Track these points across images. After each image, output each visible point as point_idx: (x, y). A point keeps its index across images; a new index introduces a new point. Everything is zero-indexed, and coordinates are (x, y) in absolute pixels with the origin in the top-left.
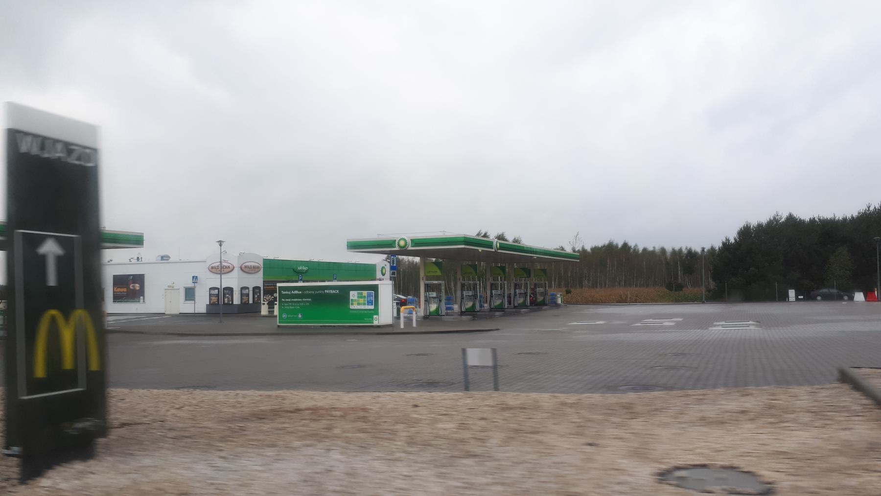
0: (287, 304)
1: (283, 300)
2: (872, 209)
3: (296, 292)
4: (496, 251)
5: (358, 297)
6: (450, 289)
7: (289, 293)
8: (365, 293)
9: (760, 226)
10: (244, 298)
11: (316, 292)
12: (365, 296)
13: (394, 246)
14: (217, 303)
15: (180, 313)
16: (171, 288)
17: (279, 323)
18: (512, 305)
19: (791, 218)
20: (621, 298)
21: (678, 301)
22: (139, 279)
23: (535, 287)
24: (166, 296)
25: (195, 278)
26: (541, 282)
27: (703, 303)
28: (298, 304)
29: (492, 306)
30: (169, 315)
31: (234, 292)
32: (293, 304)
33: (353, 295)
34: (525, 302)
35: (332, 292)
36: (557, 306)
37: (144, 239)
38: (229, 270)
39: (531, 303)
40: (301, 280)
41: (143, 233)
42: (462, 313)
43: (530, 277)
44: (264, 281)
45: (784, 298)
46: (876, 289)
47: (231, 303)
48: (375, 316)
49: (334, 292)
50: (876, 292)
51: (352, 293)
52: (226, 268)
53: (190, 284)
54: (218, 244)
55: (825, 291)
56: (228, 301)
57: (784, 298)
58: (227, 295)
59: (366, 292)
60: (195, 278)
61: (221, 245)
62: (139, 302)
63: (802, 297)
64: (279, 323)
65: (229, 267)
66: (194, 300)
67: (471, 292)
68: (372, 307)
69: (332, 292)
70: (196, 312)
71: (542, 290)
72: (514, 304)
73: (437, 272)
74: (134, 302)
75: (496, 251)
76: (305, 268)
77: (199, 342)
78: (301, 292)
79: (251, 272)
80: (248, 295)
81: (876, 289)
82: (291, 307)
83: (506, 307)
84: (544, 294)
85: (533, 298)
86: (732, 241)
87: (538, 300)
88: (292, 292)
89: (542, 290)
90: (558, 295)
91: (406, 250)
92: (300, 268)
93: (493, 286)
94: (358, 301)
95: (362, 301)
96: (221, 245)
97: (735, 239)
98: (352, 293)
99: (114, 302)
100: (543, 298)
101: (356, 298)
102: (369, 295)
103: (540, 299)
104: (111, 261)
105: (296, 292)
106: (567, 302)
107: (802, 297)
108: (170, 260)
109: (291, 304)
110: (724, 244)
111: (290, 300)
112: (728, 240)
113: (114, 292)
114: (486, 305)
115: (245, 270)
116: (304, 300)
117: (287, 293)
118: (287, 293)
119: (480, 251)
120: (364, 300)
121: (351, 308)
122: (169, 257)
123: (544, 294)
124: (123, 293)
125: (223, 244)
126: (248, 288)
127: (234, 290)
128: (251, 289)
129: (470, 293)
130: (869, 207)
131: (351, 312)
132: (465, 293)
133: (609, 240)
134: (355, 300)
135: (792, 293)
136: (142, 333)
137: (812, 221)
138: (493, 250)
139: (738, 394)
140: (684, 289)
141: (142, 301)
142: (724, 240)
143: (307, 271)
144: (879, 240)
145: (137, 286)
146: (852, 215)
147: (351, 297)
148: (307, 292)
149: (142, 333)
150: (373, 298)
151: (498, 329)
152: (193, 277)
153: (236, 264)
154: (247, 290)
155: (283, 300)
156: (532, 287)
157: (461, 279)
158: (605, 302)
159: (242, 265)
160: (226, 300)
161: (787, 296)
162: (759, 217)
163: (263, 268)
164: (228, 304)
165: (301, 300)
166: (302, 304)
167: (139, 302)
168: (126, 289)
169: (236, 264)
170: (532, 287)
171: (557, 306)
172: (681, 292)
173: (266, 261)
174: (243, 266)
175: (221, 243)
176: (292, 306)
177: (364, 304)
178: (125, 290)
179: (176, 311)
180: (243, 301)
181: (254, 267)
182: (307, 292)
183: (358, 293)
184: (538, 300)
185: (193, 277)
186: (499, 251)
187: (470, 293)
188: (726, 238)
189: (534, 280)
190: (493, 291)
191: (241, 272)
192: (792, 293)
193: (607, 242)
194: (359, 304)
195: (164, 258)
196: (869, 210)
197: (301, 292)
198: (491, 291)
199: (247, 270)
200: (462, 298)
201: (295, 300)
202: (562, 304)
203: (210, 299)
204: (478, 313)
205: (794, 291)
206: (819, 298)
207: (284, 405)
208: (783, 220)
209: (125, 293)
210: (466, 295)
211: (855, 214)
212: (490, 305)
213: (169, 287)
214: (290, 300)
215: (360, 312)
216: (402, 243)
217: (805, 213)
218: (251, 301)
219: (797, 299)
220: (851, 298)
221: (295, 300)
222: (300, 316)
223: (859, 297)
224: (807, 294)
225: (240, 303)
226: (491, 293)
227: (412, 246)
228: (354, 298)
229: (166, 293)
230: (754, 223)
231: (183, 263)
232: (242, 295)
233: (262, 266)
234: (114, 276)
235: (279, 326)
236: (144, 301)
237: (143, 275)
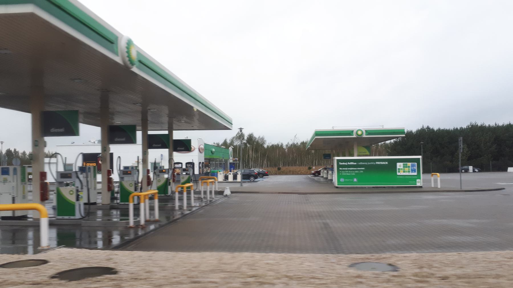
3: (352, 163)
5: (404, 167)
8: (409, 164)
11: (369, 163)
12: (409, 166)
13: (352, 134)
19: (428, 128)
28: (354, 172)
32: (350, 172)
33: (399, 165)
35: (382, 163)
44: (205, 159)
48: (418, 180)
61: (2, 144)
68: (416, 174)
69: (382, 163)
73: (366, 152)
78: (355, 164)
82: (348, 174)
91: (362, 137)
94: (404, 169)
95: (407, 169)
96: (2, 144)
101: (402, 167)
102: (412, 166)
105: (352, 163)
116: (343, 169)
120: (409, 169)
125: (4, 143)
126: (181, 163)
127: (195, 164)
131: (398, 177)
134: (401, 169)
135: (471, 168)
147: (398, 167)
148: (361, 163)
150: (416, 168)
154: (181, 165)
155: (340, 169)
168: (95, 164)
177: (409, 172)
182: (361, 163)
183: (404, 164)
194: (404, 172)
197: (355, 164)
205: (472, 167)
211: (436, 129)
214: (346, 169)
215: (406, 177)
216: (360, 133)
217: (435, 127)
219: (474, 171)
222: (355, 180)
227: (366, 135)
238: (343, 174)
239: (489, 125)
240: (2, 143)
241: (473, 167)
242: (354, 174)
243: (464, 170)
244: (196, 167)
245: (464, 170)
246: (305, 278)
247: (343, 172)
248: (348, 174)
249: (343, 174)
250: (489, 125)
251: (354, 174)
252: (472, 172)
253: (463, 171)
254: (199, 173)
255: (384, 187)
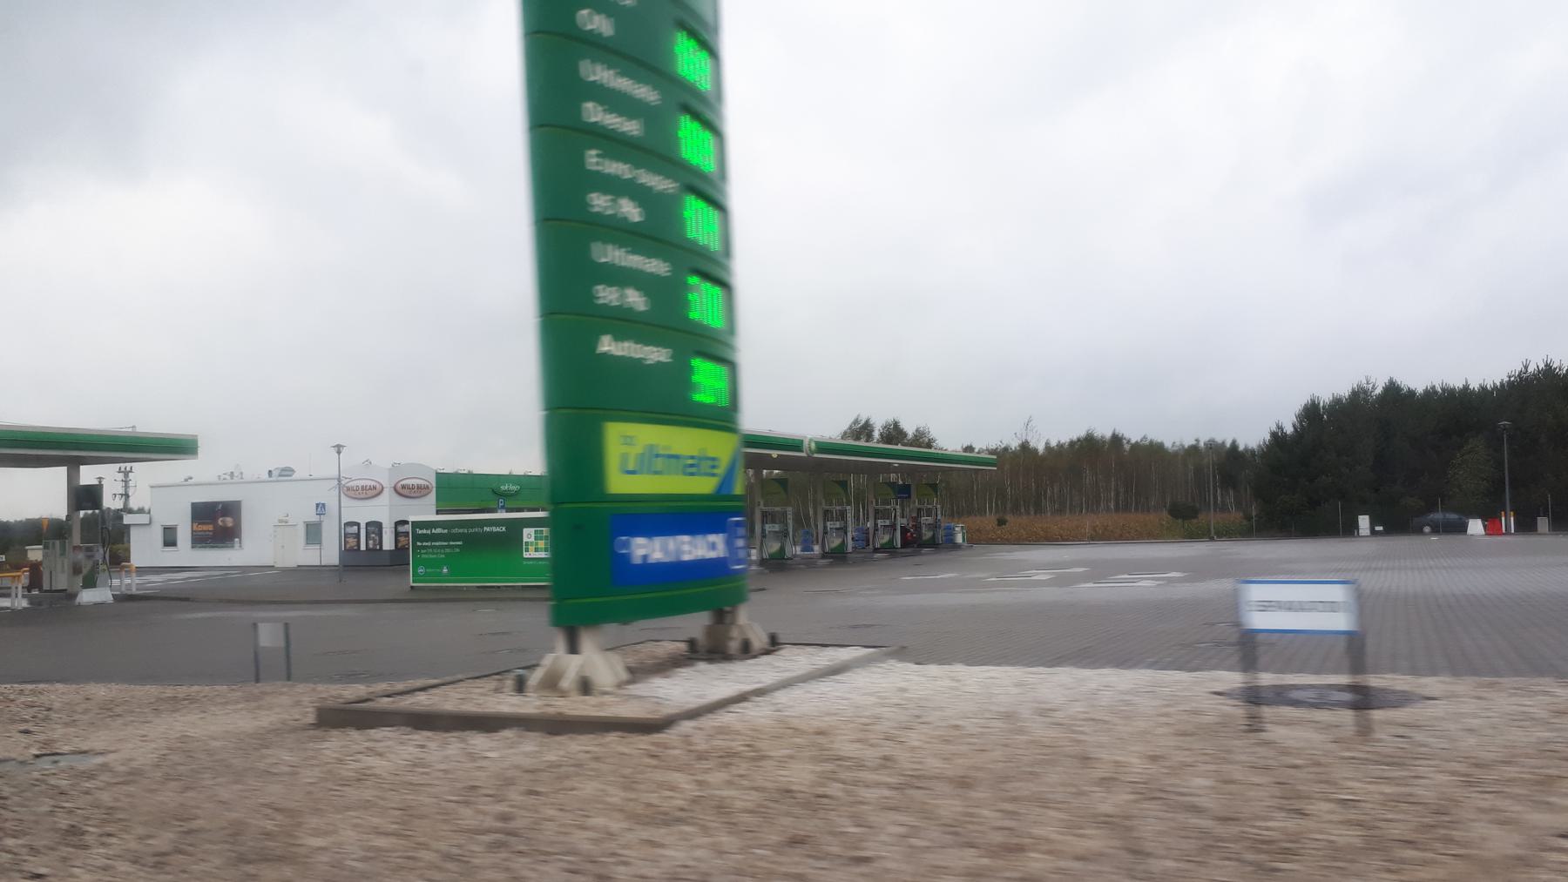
0: (425, 551)
1: (419, 544)
2: (1531, 369)
3: (439, 531)
4: (809, 456)
6: (807, 517)
7: (429, 532)
9: (1337, 401)
10: (402, 539)
11: (471, 531)
14: (356, 548)
15: (299, 566)
16: (283, 523)
17: (413, 582)
18: (871, 546)
19: (1392, 389)
20: (1095, 531)
21: (1193, 536)
22: (230, 509)
23: (919, 515)
24: (275, 536)
25: (321, 508)
26: (888, 507)
27: (1212, 539)
28: (442, 551)
29: (765, 556)
30: (277, 569)
31: (384, 530)
32: (435, 551)
34: (891, 541)
36: (957, 547)
37: (199, 445)
38: (374, 492)
39: (905, 544)
40: (503, 507)
41: (196, 436)
42: (762, 562)
43: (909, 497)
45: (1350, 530)
46: (1503, 513)
47: (378, 547)
49: (498, 529)
50: (1503, 519)
51: (526, 531)
52: (370, 489)
53: (315, 518)
54: (334, 452)
55: (1438, 516)
56: (375, 545)
57: (1350, 530)
58: (373, 535)
59: (533, 529)
60: (321, 508)
61: (339, 453)
62: (233, 547)
63: (1381, 528)
64: (413, 582)
65: (375, 488)
66: (320, 543)
67: (838, 523)
69: (495, 529)
70: (323, 564)
71: (930, 520)
72: (874, 547)
74: (222, 547)
75: (809, 456)
76: (514, 488)
77: (219, 614)
78: (446, 531)
79: (412, 495)
80: (358, 536)
81: (1503, 513)
82: (431, 556)
83: (850, 549)
84: (934, 527)
85: (912, 534)
86: (1289, 430)
87: (924, 538)
88: (433, 531)
89: (930, 520)
90: (957, 529)
92: (504, 488)
93: (885, 514)
94: (537, 544)
96: (339, 453)
97: (1294, 426)
98: (526, 531)
99: (193, 547)
100: (932, 533)
101: (533, 539)
103: (927, 534)
104: (191, 478)
106: (975, 539)
107: (1381, 528)
108: (294, 477)
109: (431, 550)
110: (1274, 435)
111: (429, 544)
112: (1280, 428)
113: (193, 531)
114: (754, 552)
115: (405, 492)
117: (425, 531)
118: (425, 531)
119: (775, 456)
121: (525, 556)
122: (293, 471)
123: (934, 527)
124: (207, 533)
125: (344, 451)
127: (384, 526)
128: (363, 526)
129: (777, 527)
130: (1526, 367)
132: (880, 522)
133: (1087, 429)
135: (1364, 522)
136: (187, 599)
137: (1430, 394)
138: (803, 454)
139: (536, 695)
140: (1201, 517)
141: (237, 545)
142: (1274, 428)
143: (517, 492)
144: (1507, 426)
145: (229, 521)
146: (1503, 380)
147: (525, 539)
149: (187, 599)
151: (764, 589)
152: (317, 505)
153: (387, 483)
154: (356, 527)
155: (419, 544)
156: (914, 515)
157: (762, 503)
158: (1057, 540)
159: (397, 483)
160: (371, 542)
161: (1356, 526)
162: (1333, 386)
163: (438, 487)
164: (374, 550)
165: (446, 544)
166: (448, 550)
167: (233, 547)
169: (387, 483)
170: (914, 515)
171: (957, 547)
172: (1195, 521)
173: (440, 476)
174: (399, 485)
175: (339, 449)
176: (433, 554)
178: (210, 527)
179: (291, 562)
180: (400, 545)
181: (419, 487)
182: (456, 531)
184: (924, 538)
185: (317, 505)
186: (816, 455)
187: (777, 527)
188: (1278, 426)
189: (874, 503)
190: (828, 523)
191: (395, 495)
192: (1364, 522)
193: (1082, 433)
194: (536, 550)
195: (286, 472)
196: (1527, 371)
197: (446, 531)
198: (825, 523)
199: (405, 492)
200: (764, 536)
201: (437, 544)
202: (966, 544)
203: (397, 541)
204: (789, 562)
206: (1427, 529)
207: (1419, 737)
208: (1379, 391)
209: (211, 533)
210: (769, 532)
212: (823, 546)
213: (280, 521)
214: (429, 544)
217: (1417, 380)
218: (363, 547)
219: (1373, 533)
220: (1462, 529)
221: (437, 544)
222: (445, 570)
223: (1476, 526)
224: (1395, 522)
225: (393, 548)
226: (825, 527)
228: (533, 535)
229: (275, 531)
230: (1325, 397)
231: (190, 487)
232: (397, 534)
233: (434, 485)
234: (193, 504)
235: (412, 587)
236: (240, 546)
237: (193, 504)
238: (423, 556)
239: (1234, 442)
240: (339, 449)
241: (1482, 520)
242: (443, 556)
243: (1431, 527)
244: (386, 533)
245: (1428, 525)
246: (1247, 750)
247: (422, 551)
248: (431, 556)
249: (423, 556)
250: (1234, 442)
251: (443, 556)
252: (1369, 534)
253: (1427, 529)
254: (396, 546)
255: (499, 587)
